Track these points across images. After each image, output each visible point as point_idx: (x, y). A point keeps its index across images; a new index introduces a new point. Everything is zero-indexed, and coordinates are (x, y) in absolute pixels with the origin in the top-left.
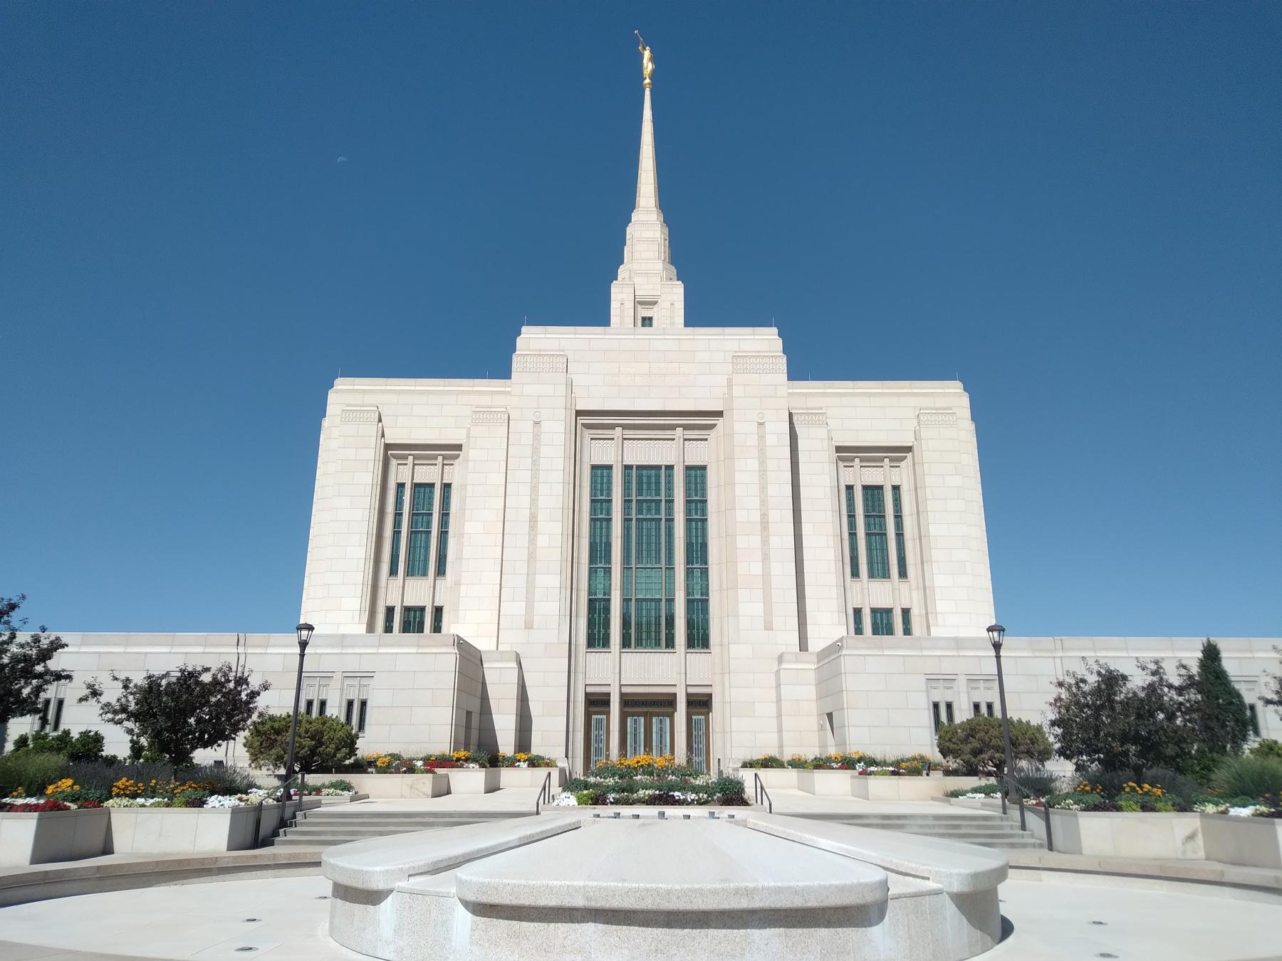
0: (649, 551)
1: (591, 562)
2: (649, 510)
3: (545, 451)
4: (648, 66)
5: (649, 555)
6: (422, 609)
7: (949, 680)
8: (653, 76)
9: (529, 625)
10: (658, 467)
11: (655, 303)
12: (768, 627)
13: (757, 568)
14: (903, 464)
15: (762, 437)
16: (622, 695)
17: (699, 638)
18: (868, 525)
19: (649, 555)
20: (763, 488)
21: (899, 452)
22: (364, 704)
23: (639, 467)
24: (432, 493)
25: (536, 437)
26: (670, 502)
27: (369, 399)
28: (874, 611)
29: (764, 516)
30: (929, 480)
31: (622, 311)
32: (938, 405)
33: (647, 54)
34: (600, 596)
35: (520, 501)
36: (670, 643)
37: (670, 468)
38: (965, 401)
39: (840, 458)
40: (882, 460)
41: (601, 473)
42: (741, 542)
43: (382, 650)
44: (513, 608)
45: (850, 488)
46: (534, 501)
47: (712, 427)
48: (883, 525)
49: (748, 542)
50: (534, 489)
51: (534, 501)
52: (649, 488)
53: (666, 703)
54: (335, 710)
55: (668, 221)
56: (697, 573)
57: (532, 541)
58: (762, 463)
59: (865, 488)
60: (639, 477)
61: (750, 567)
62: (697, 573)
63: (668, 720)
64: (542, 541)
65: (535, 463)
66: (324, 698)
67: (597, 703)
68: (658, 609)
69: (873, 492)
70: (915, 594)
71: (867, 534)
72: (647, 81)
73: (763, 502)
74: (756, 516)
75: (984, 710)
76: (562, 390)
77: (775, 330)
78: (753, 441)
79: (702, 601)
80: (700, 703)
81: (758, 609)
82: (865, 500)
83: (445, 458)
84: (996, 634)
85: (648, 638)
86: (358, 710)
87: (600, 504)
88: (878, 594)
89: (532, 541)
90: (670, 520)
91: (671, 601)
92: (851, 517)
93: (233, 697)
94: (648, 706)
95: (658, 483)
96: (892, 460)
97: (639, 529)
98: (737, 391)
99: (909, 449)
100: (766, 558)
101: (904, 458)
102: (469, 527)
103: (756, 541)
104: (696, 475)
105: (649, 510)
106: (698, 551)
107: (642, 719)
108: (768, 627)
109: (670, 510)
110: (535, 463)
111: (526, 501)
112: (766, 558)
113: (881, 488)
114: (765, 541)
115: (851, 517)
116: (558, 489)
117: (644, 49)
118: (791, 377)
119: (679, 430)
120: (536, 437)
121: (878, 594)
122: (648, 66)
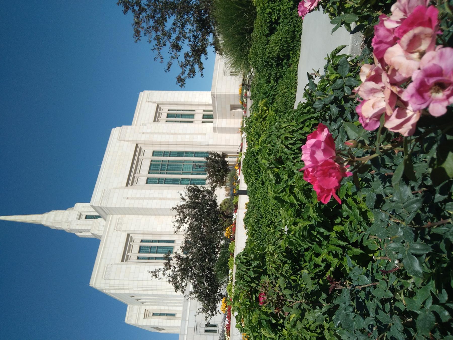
0: (177, 168)
1: (183, 156)
2: (164, 168)
3: (138, 196)
7: (197, 324)
10: (151, 165)
11: (81, 214)
13: (188, 136)
14: (133, 238)
15: (147, 133)
18: (154, 253)
20: (164, 134)
21: (158, 108)
23: (150, 169)
25: (132, 198)
26: (163, 161)
27: (101, 270)
29: (172, 134)
30: (168, 100)
31: (80, 225)
34: (190, 182)
37: (152, 161)
39: (126, 261)
40: (159, 113)
41: (149, 181)
43: (187, 319)
45: (138, 258)
46: (155, 199)
47: (141, 149)
48: (154, 247)
49: (179, 139)
50: (151, 199)
51: (155, 199)
55: (48, 210)
57: (169, 199)
58: (156, 133)
59: (139, 252)
61: (187, 139)
64: (169, 196)
65: (141, 198)
69: (168, 116)
71: (157, 253)
73: (168, 134)
74: (172, 136)
81: (199, 137)
82: (144, 252)
83: (131, 241)
87: (160, 181)
88: (199, 117)
90: (169, 161)
92: (149, 258)
95: (156, 165)
96: (131, 241)
97: (170, 170)
99: (128, 235)
101: (160, 108)
102: (159, 229)
103: (179, 136)
104: (155, 153)
105: (164, 168)
106: (180, 154)
108: (205, 134)
109: (165, 161)
110: (141, 198)
111: (155, 201)
113: (140, 247)
114: (180, 134)
115: (149, 258)
118: (131, 125)
119: (139, 157)
120: (132, 198)
121: (199, 117)
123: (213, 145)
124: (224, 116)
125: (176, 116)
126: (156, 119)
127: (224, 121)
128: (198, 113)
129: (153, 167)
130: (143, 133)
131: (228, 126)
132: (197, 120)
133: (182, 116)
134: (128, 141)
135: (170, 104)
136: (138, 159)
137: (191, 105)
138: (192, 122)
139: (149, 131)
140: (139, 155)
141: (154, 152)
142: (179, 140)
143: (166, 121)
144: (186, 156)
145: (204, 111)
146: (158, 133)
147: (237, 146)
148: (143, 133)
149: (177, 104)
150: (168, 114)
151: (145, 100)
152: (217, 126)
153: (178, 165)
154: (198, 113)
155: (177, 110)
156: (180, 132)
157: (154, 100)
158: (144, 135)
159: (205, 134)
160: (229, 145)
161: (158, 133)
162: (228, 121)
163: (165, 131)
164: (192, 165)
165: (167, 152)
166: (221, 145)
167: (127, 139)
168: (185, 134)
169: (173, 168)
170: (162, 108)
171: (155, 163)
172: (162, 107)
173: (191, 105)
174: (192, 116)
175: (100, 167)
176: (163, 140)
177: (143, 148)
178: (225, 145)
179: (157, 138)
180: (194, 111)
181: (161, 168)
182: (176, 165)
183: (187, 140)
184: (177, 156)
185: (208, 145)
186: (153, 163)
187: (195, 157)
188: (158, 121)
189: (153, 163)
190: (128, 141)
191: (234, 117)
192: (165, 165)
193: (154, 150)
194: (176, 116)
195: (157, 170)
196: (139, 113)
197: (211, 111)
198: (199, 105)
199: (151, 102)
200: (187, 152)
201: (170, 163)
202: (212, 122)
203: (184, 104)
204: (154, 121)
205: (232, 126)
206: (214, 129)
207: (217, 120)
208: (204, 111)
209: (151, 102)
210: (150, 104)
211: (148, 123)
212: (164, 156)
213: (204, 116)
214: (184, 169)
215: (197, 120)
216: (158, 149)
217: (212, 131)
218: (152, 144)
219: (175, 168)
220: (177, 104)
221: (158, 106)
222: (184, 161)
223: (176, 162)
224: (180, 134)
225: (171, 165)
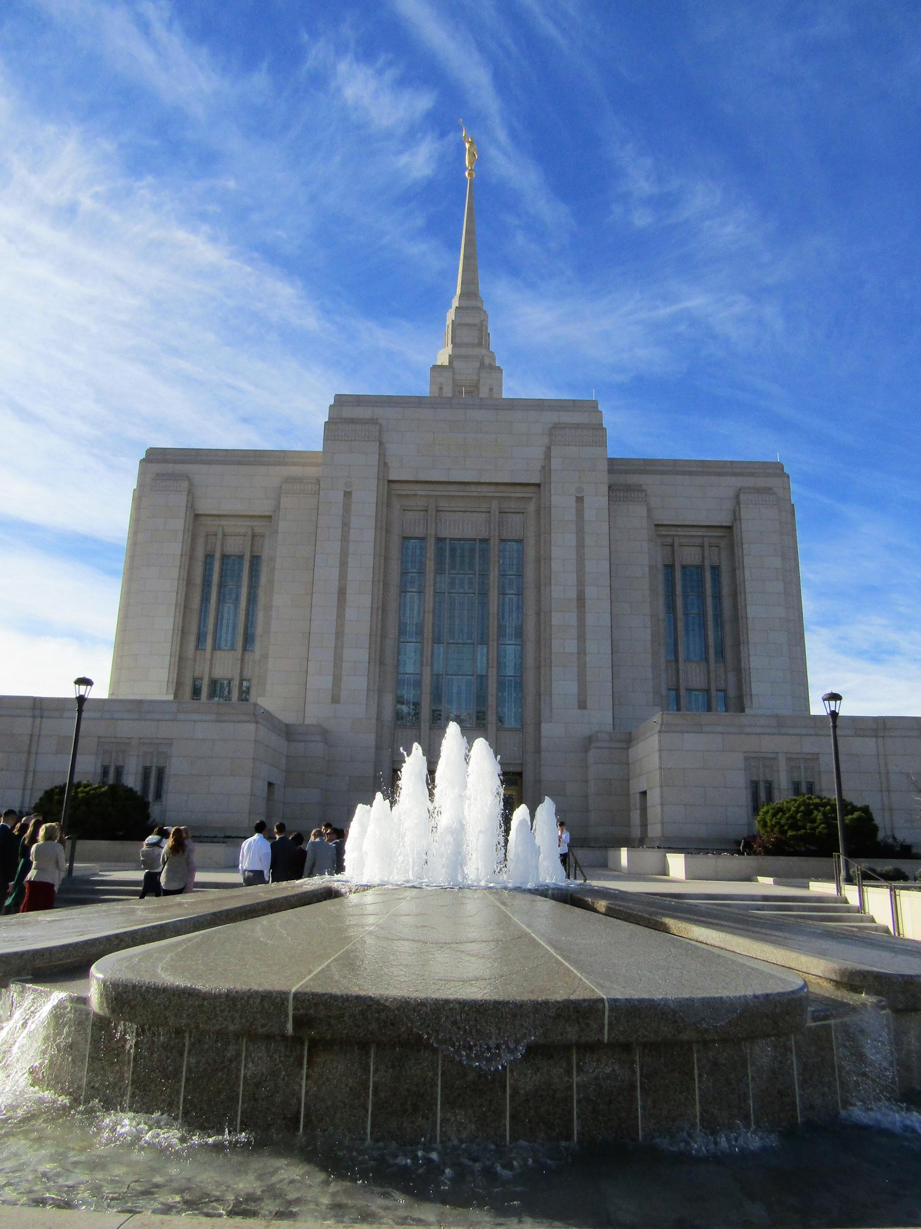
3: (355, 522)
6: (241, 557)
9: (335, 699)
12: (582, 705)
13: (572, 646)
22: (161, 772)
24: (241, 565)
35: (328, 573)
37: (485, 541)
42: (556, 619)
44: (320, 682)
50: (343, 565)
54: (132, 781)
57: (341, 616)
60: (453, 550)
64: (350, 614)
66: (120, 764)
74: (573, 594)
75: (804, 788)
76: (374, 459)
77: (360, 806)
78: (571, 515)
84: (832, 703)
86: (156, 777)
89: (341, 616)
93: (116, 999)
98: (555, 464)
100: (581, 638)
103: (572, 618)
108: (582, 705)
112: (581, 638)
116: (369, 561)
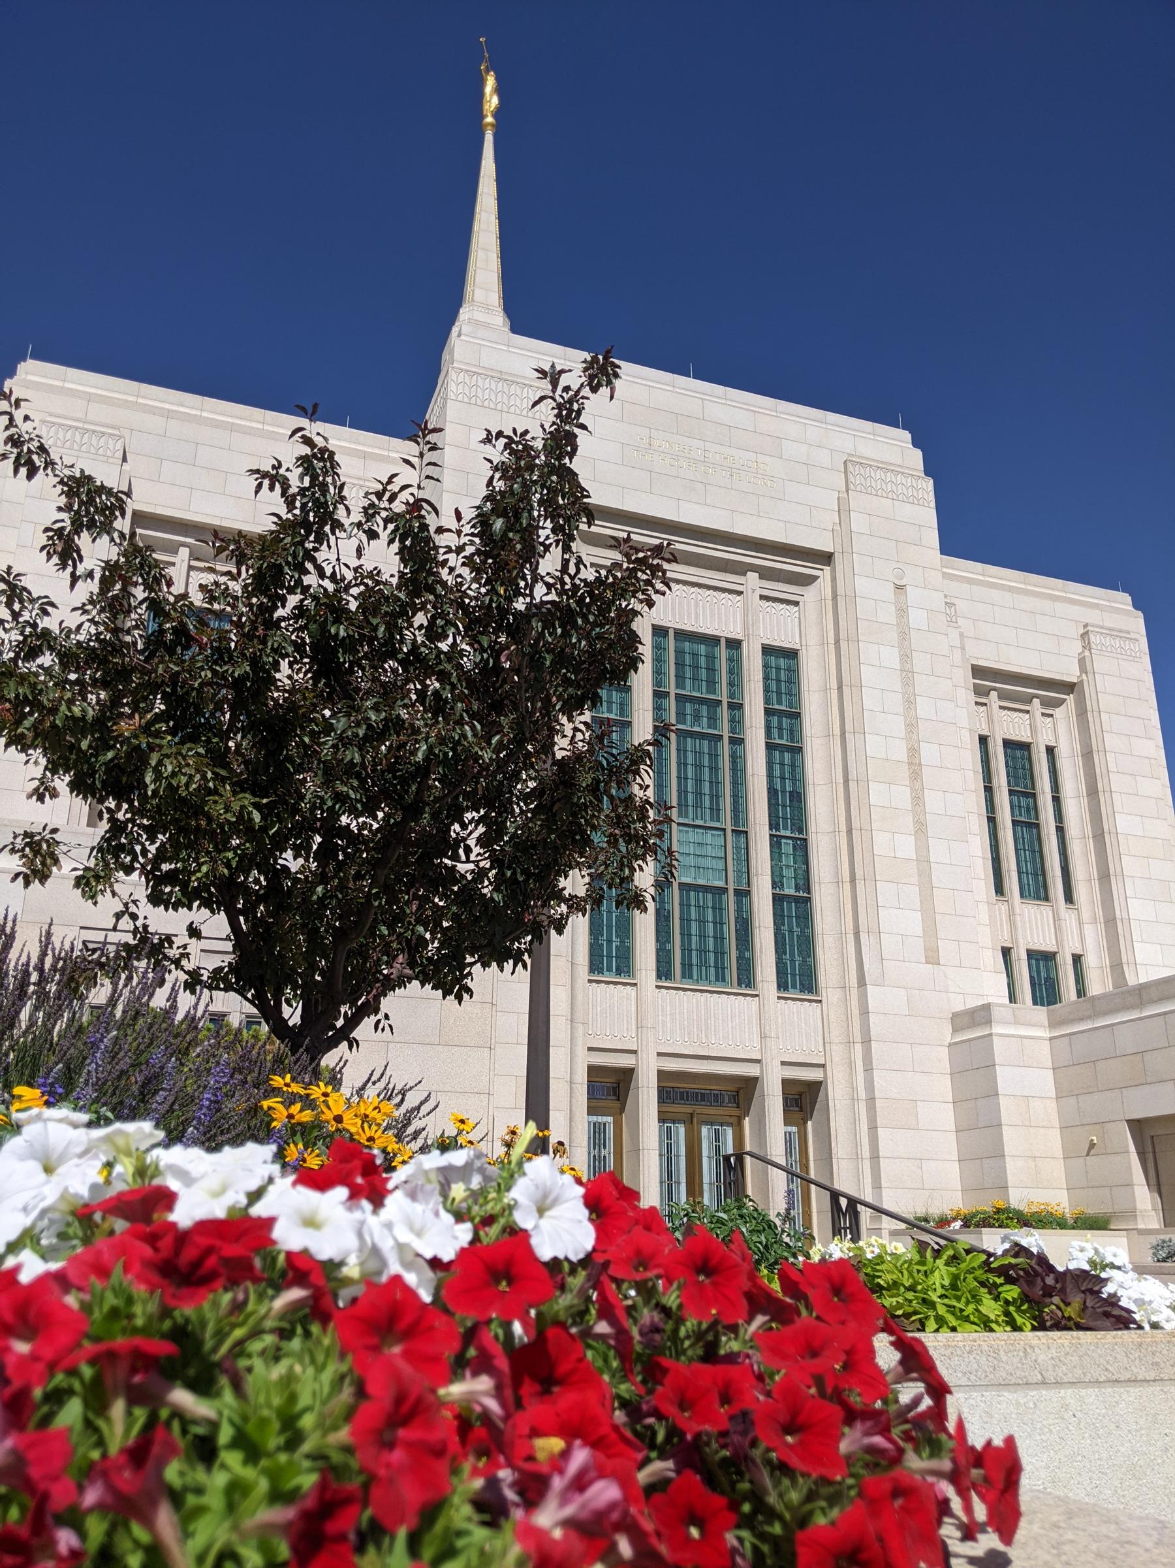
0: (699, 794)
2: (697, 717)
4: (492, 101)
5: (698, 805)
8: (497, 114)
10: (714, 641)
13: (906, 846)
15: (902, 611)
16: (662, 1075)
17: (798, 976)
19: (698, 805)
20: (910, 703)
21: (1055, 690)
23: (681, 635)
26: (736, 707)
28: (1031, 954)
29: (913, 751)
32: (1107, 624)
33: (490, 82)
36: (746, 978)
37: (734, 644)
38: (1136, 623)
47: (808, 580)
49: (885, 796)
52: (695, 678)
53: (739, 1094)
56: (787, 847)
61: (891, 843)
62: (787, 847)
63: (729, 1132)
67: (610, 1087)
68: (718, 909)
69: (1017, 750)
70: (1089, 930)
72: (489, 119)
73: (911, 727)
74: (900, 752)
78: (888, 614)
79: (796, 899)
80: (803, 1099)
81: (913, 922)
85: (703, 963)
88: (1036, 927)
90: (737, 741)
91: (743, 894)
94: (707, 1098)
95: (711, 670)
98: (858, 522)
101: (1059, 703)
103: (902, 795)
104: (782, 662)
106: (789, 805)
107: (682, 1129)
108: (932, 958)
109: (737, 722)
114: (918, 799)
117: (487, 72)
119: (752, 576)
121: (1036, 927)
122: (492, 101)
123: (865, 1012)
124: (1075, 1077)
125: (1023, 794)
126: (988, 680)
127: (1044, 1081)
128: (1057, 920)
129: (695, 655)
130: (900, 588)
131: (1008, 1109)
132: (1011, 915)
133: (1027, 826)
134: (843, 509)
135: (1088, 755)
136: (741, 569)
137: (1105, 877)
138: (999, 889)
139: (917, 618)
140: (766, 574)
141: (792, 655)
142: (877, 793)
143: (983, 740)
144: (775, 842)
145: (1077, 959)
146: (907, 674)
147: (877, 1186)
148: (900, 588)
149: (1093, 792)
150: (1025, 747)
151: (1093, 617)
152: (996, 1029)
153: (715, 797)
154: (1057, 920)
155: (1056, 799)
156: (933, 801)
157: (1100, 664)
158: (889, 592)
159: (932, 958)
160: (873, 1128)
161: (907, 674)
162: (1047, 1110)
163: (924, 708)
164: (721, 884)
165: (796, 733)
166: (869, 1069)
167: (857, 500)
168: (921, 830)
169: (698, 766)
170: (1059, 712)
171: (723, 666)
172: (1066, 713)
173: (1105, 877)
174: (1036, 888)
175: (686, 374)
176: (870, 700)
177: (809, 595)
178: (871, 1100)
179: (877, 665)
180: (1069, 898)
181: (691, 699)
182: (715, 783)
183: (881, 840)
184: (772, 792)
185: (862, 983)
186: (723, 652)
187: (778, 900)
188: (979, 691)
189: (723, 652)
190: (843, 509)
191: (1085, 1148)
192: (713, 721)
193: (803, 657)
194: (1023, 794)
195: (680, 678)
196: (1010, 589)
197: (1081, 992)
198: (1111, 922)
199: (1087, 646)
200: (802, 847)
201: (725, 748)
202: (1012, 998)
203: (1099, 837)
204: (978, 672)
205: (1011, 1139)
206: (981, 1015)
207: (1046, 1034)
208: (1077, 959)
209: (1087, 646)
210: (1077, 647)
211: (961, 635)
212: (768, 712)
213: (1042, 960)
214: (691, 835)
215: (1011, 915)
216: (813, 677)
217: (960, 1004)
218: (839, 644)
219: (698, 781)
220: (1093, 792)
221: (1069, 687)
222: (742, 833)
223: (735, 783)
224: (918, 799)
225: (714, 756)
